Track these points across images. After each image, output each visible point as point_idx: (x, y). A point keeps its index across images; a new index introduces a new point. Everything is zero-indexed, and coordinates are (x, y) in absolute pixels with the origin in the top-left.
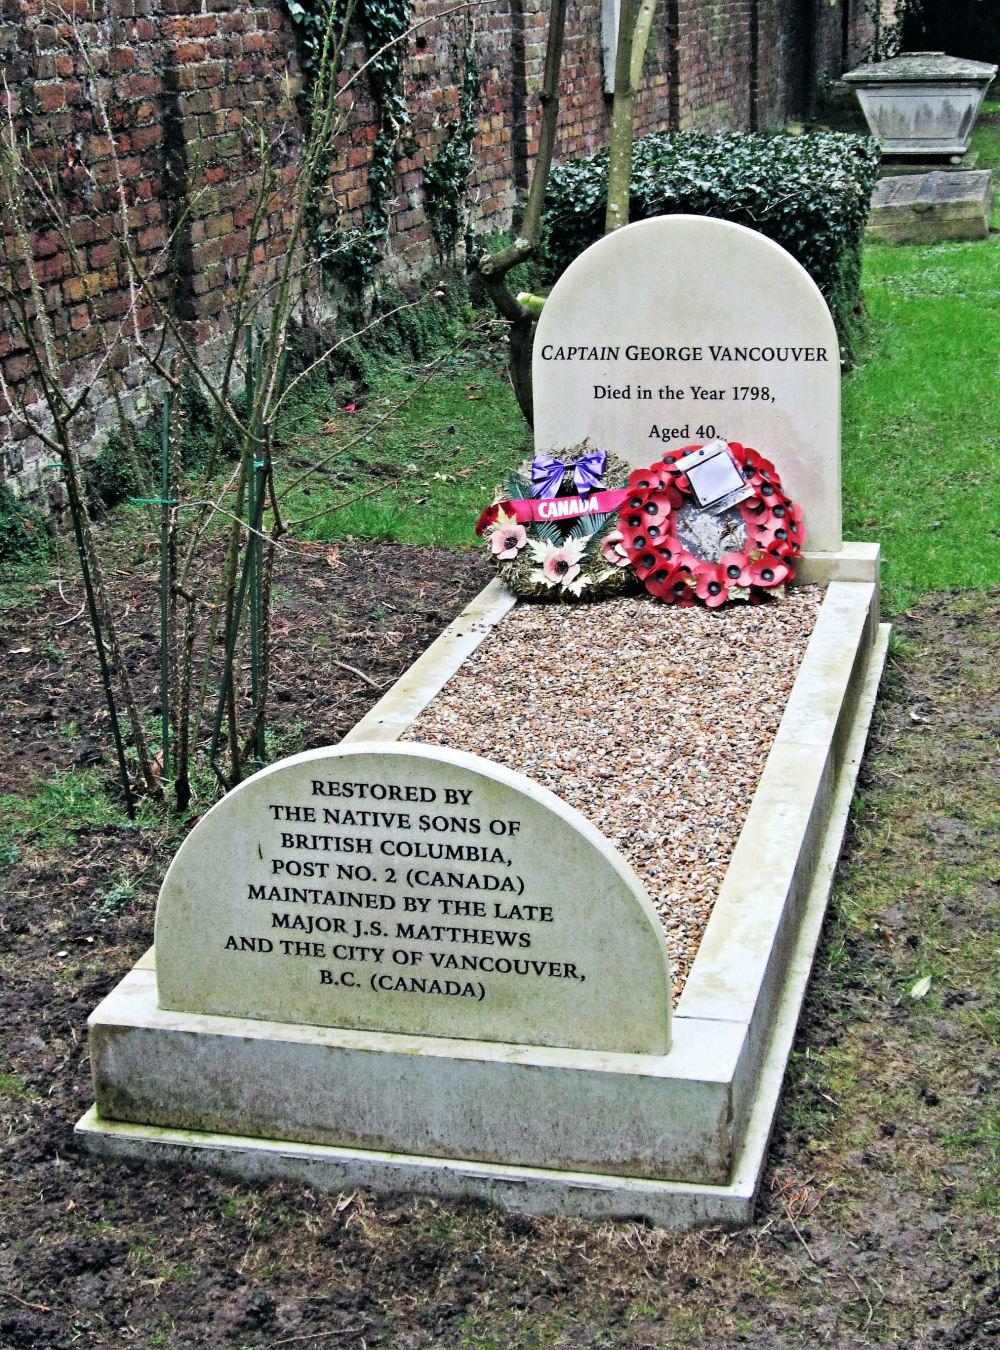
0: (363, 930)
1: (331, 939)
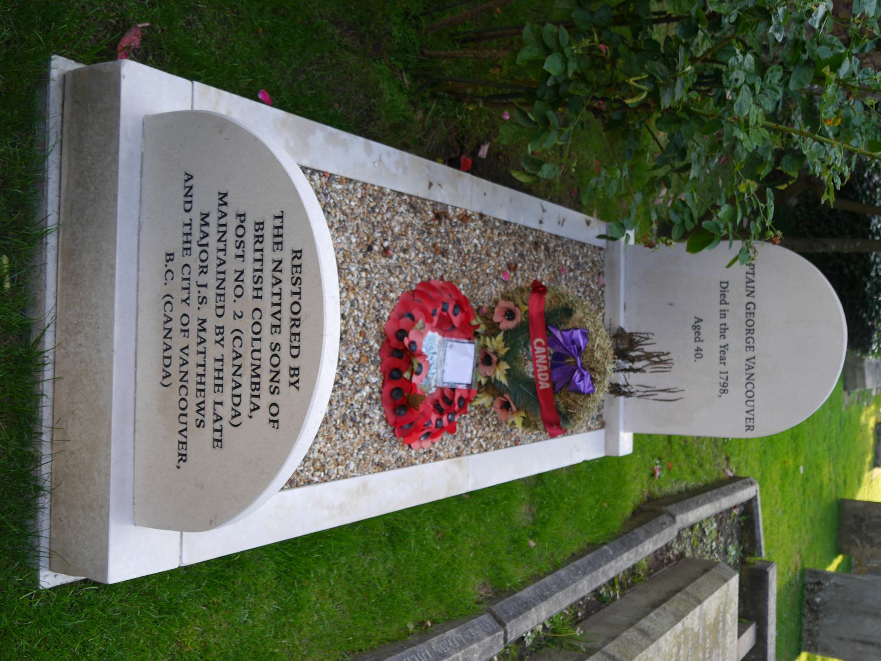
0: (201, 289)
1: (194, 261)
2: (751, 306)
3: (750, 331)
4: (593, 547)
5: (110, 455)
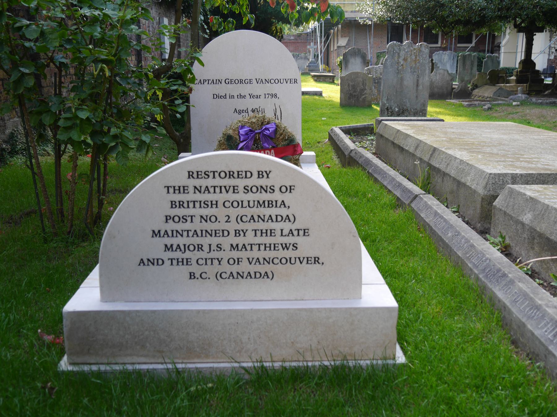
0: (212, 249)
1: (193, 255)
2: (227, 81)
3: (241, 81)
4: (370, 175)
5: (318, 309)
